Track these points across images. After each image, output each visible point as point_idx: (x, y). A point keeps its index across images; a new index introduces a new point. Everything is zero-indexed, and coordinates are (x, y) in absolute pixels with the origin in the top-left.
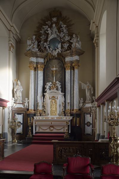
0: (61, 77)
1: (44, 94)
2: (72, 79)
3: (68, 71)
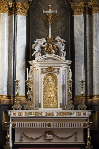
0: (64, 28)
1: (30, 62)
2: (88, 32)
3: (78, 16)
